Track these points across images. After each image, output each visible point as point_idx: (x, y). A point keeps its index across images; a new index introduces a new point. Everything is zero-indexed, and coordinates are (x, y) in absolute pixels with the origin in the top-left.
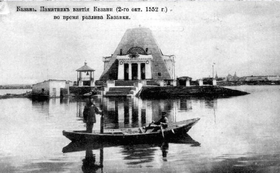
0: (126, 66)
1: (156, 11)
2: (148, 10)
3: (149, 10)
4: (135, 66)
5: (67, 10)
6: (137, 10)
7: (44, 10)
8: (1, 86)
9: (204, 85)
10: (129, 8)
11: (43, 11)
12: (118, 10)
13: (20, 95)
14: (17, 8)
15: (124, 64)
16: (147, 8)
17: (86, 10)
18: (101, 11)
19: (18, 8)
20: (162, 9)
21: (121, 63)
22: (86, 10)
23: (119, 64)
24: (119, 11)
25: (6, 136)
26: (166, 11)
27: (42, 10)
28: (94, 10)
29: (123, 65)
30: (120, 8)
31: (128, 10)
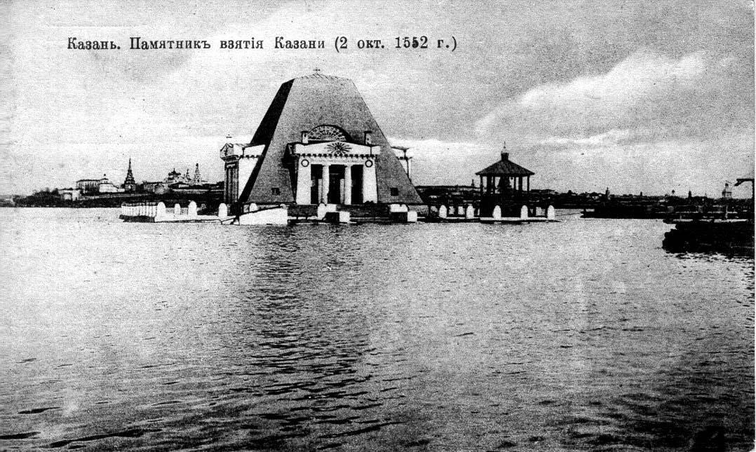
0: (317, 171)
1: (422, 47)
2: (401, 44)
3: (405, 45)
4: (337, 172)
5: (202, 45)
6: (372, 44)
7: (140, 46)
8: (2, 201)
9: (448, 218)
10: (348, 38)
11: (138, 48)
12: (339, 44)
13: (135, 217)
14: (68, 41)
15: (312, 165)
16: (398, 39)
17: (255, 45)
18: (229, 47)
19: (278, 40)
20: (439, 41)
21: (305, 163)
22: (255, 45)
23: (300, 165)
24: (342, 47)
25: (644, 268)
26: (452, 46)
27: (135, 46)
28: (69, 45)
29: (309, 169)
30: (345, 38)
31: (359, 45)
